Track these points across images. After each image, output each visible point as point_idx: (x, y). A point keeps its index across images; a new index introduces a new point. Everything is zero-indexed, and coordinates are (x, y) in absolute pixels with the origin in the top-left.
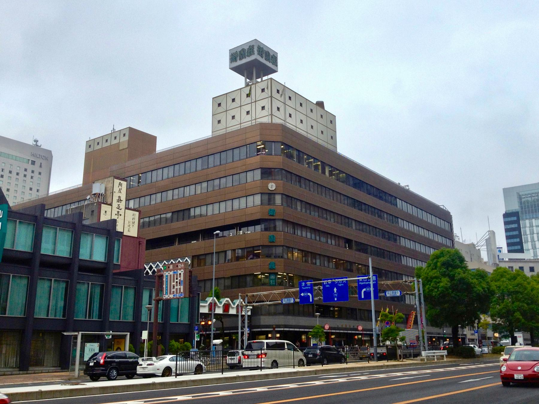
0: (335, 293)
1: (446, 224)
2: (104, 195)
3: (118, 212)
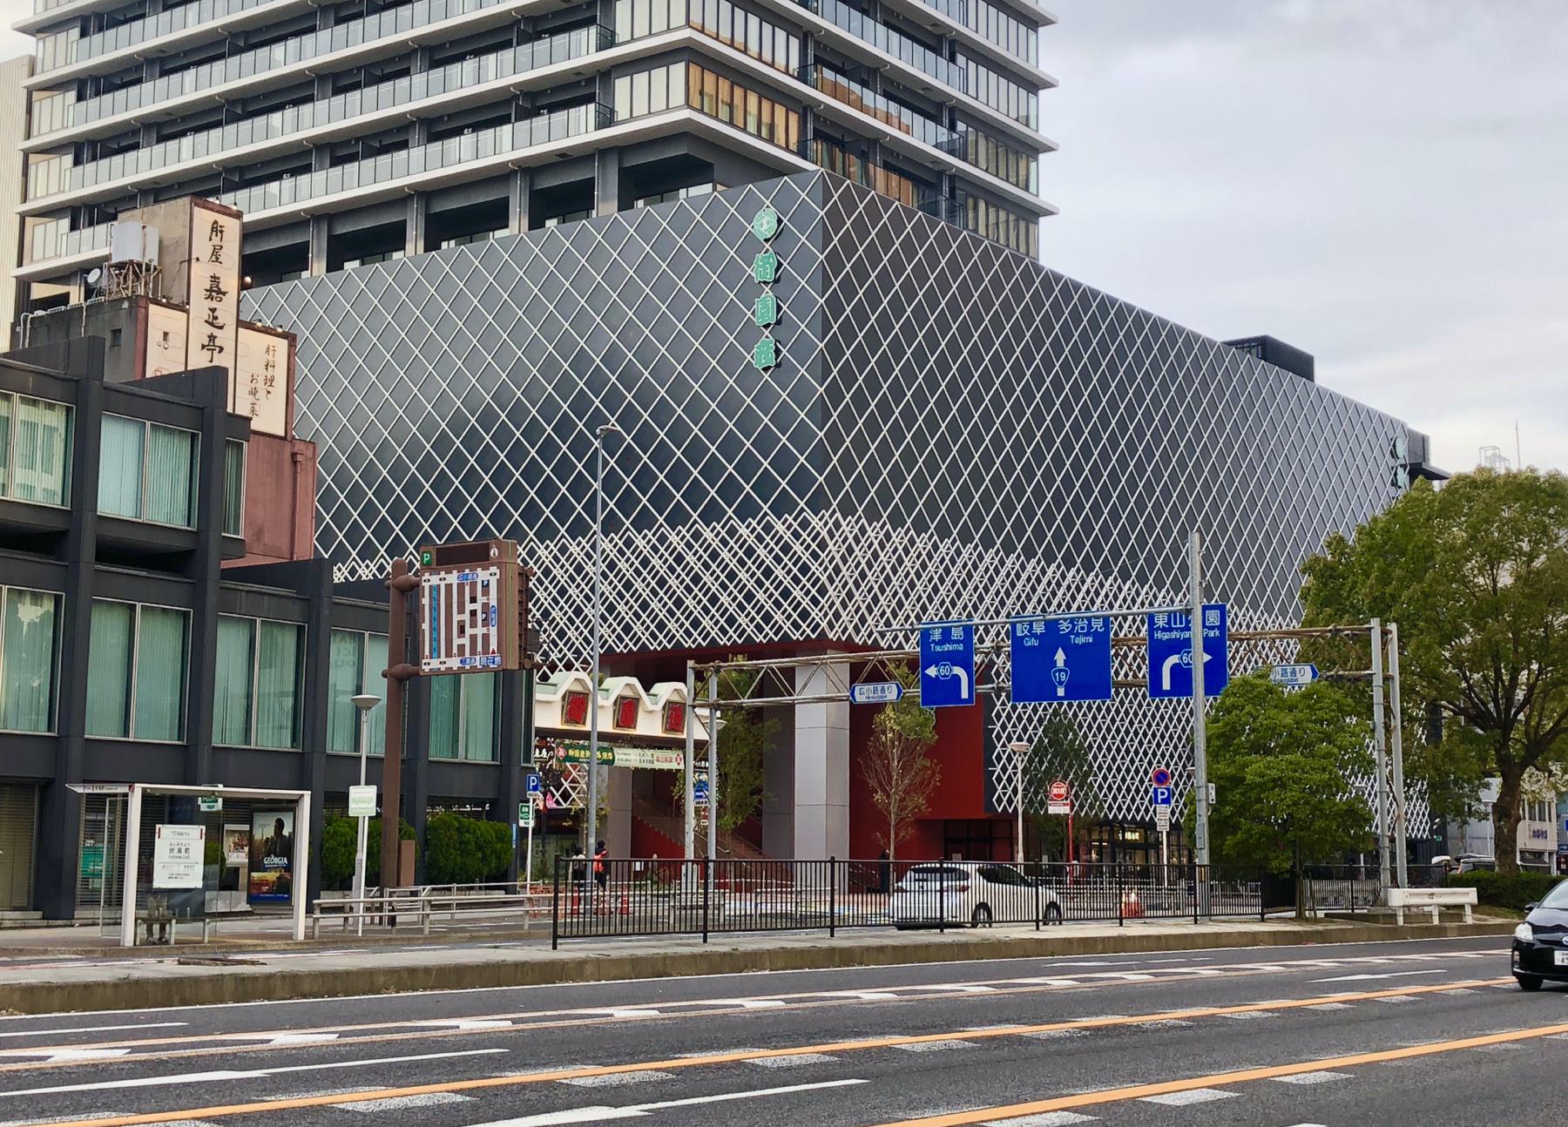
0: (1060, 671)
2: (155, 268)
3: (212, 338)
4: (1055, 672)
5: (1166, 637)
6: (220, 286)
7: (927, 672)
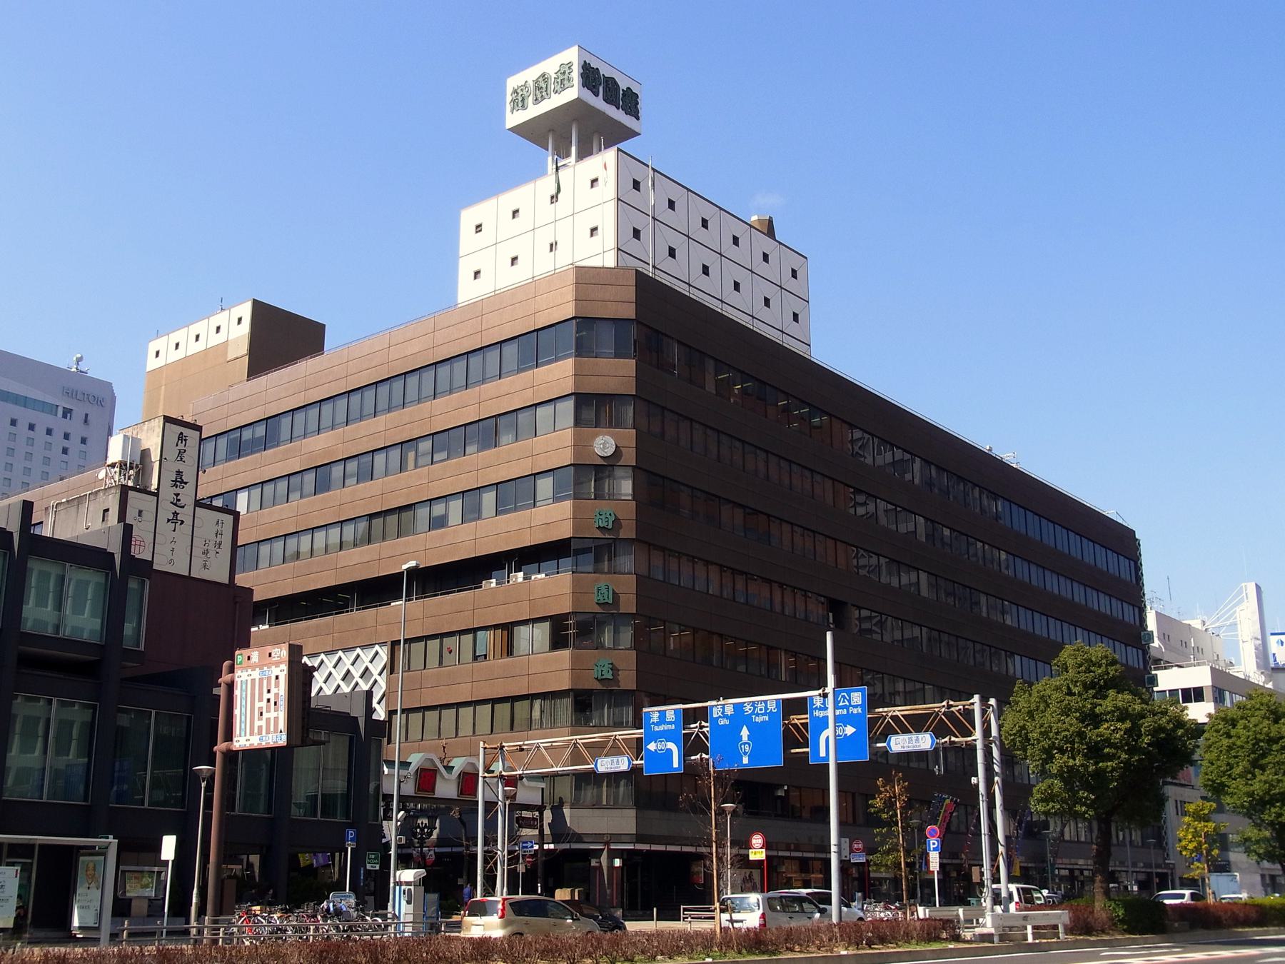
0: (745, 744)
1: (1124, 562)
3: (175, 514)
4: (741, 745)
5: (822, 715)
6: (183, 478)
7: (648, 747)
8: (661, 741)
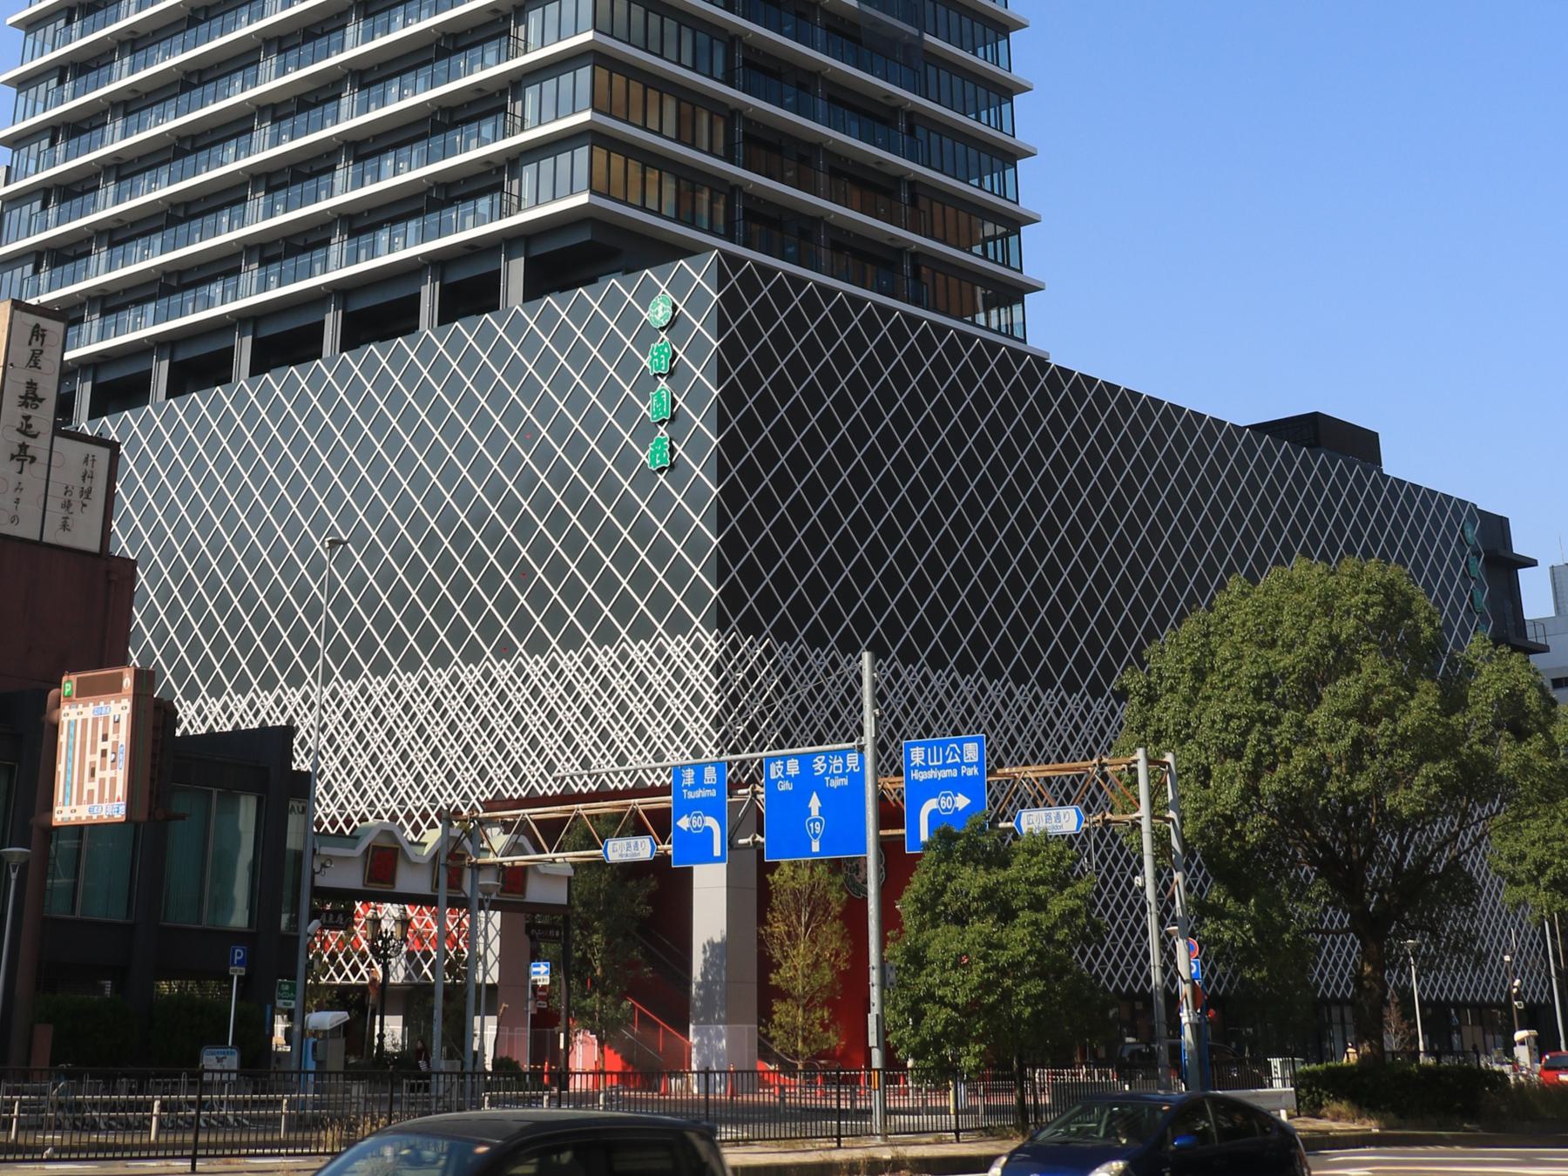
0: (815, 820)
3: (23, 447)
6: (38, 392)
8: (946, 796)
